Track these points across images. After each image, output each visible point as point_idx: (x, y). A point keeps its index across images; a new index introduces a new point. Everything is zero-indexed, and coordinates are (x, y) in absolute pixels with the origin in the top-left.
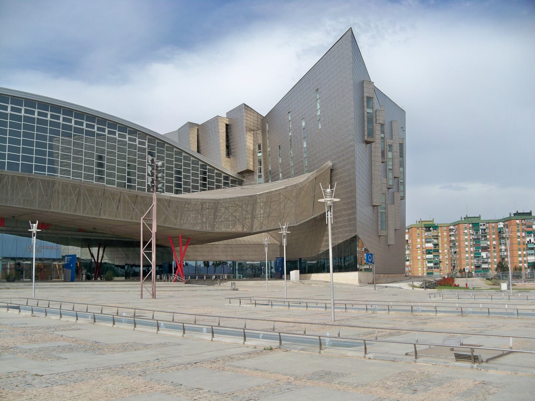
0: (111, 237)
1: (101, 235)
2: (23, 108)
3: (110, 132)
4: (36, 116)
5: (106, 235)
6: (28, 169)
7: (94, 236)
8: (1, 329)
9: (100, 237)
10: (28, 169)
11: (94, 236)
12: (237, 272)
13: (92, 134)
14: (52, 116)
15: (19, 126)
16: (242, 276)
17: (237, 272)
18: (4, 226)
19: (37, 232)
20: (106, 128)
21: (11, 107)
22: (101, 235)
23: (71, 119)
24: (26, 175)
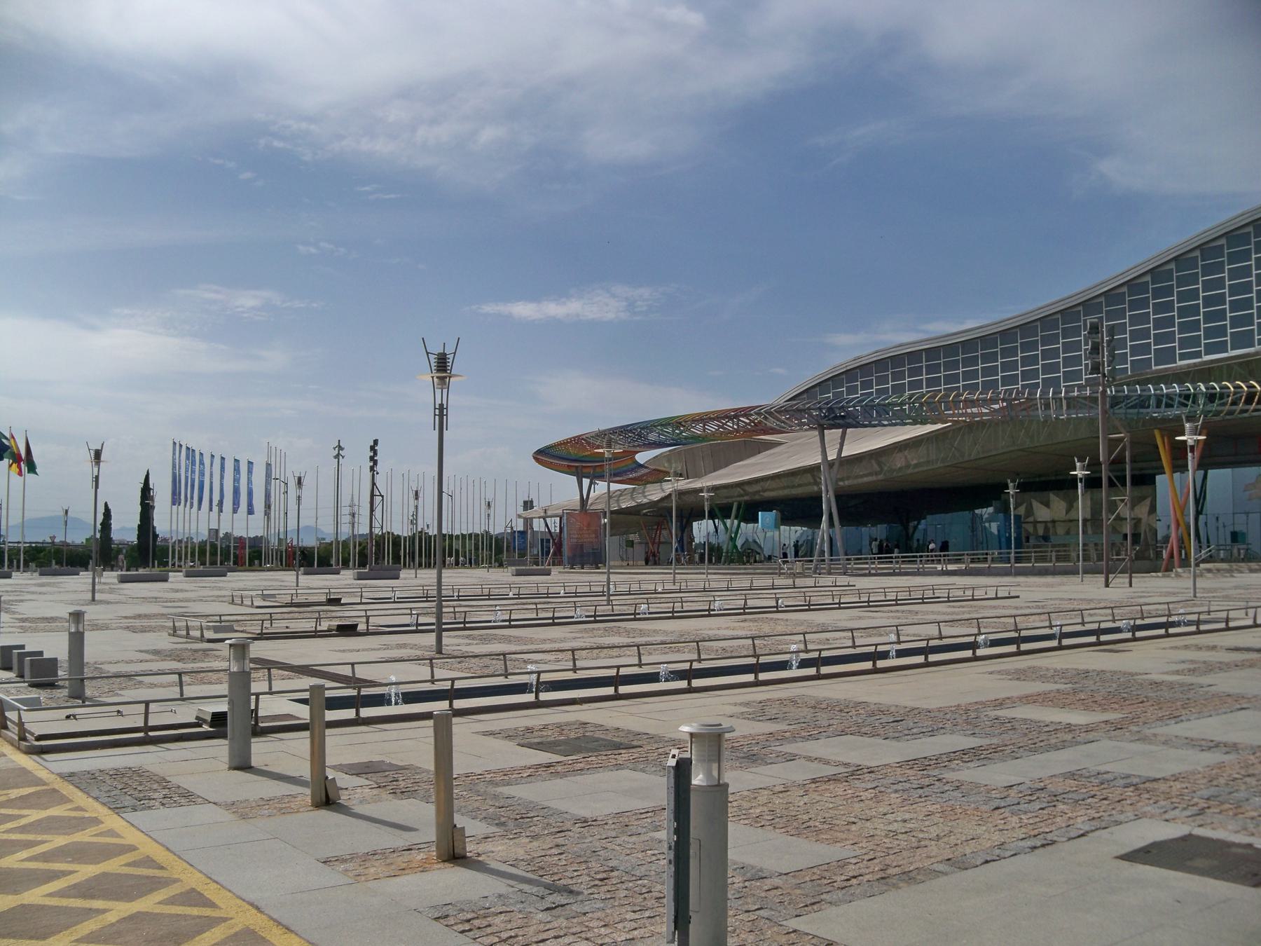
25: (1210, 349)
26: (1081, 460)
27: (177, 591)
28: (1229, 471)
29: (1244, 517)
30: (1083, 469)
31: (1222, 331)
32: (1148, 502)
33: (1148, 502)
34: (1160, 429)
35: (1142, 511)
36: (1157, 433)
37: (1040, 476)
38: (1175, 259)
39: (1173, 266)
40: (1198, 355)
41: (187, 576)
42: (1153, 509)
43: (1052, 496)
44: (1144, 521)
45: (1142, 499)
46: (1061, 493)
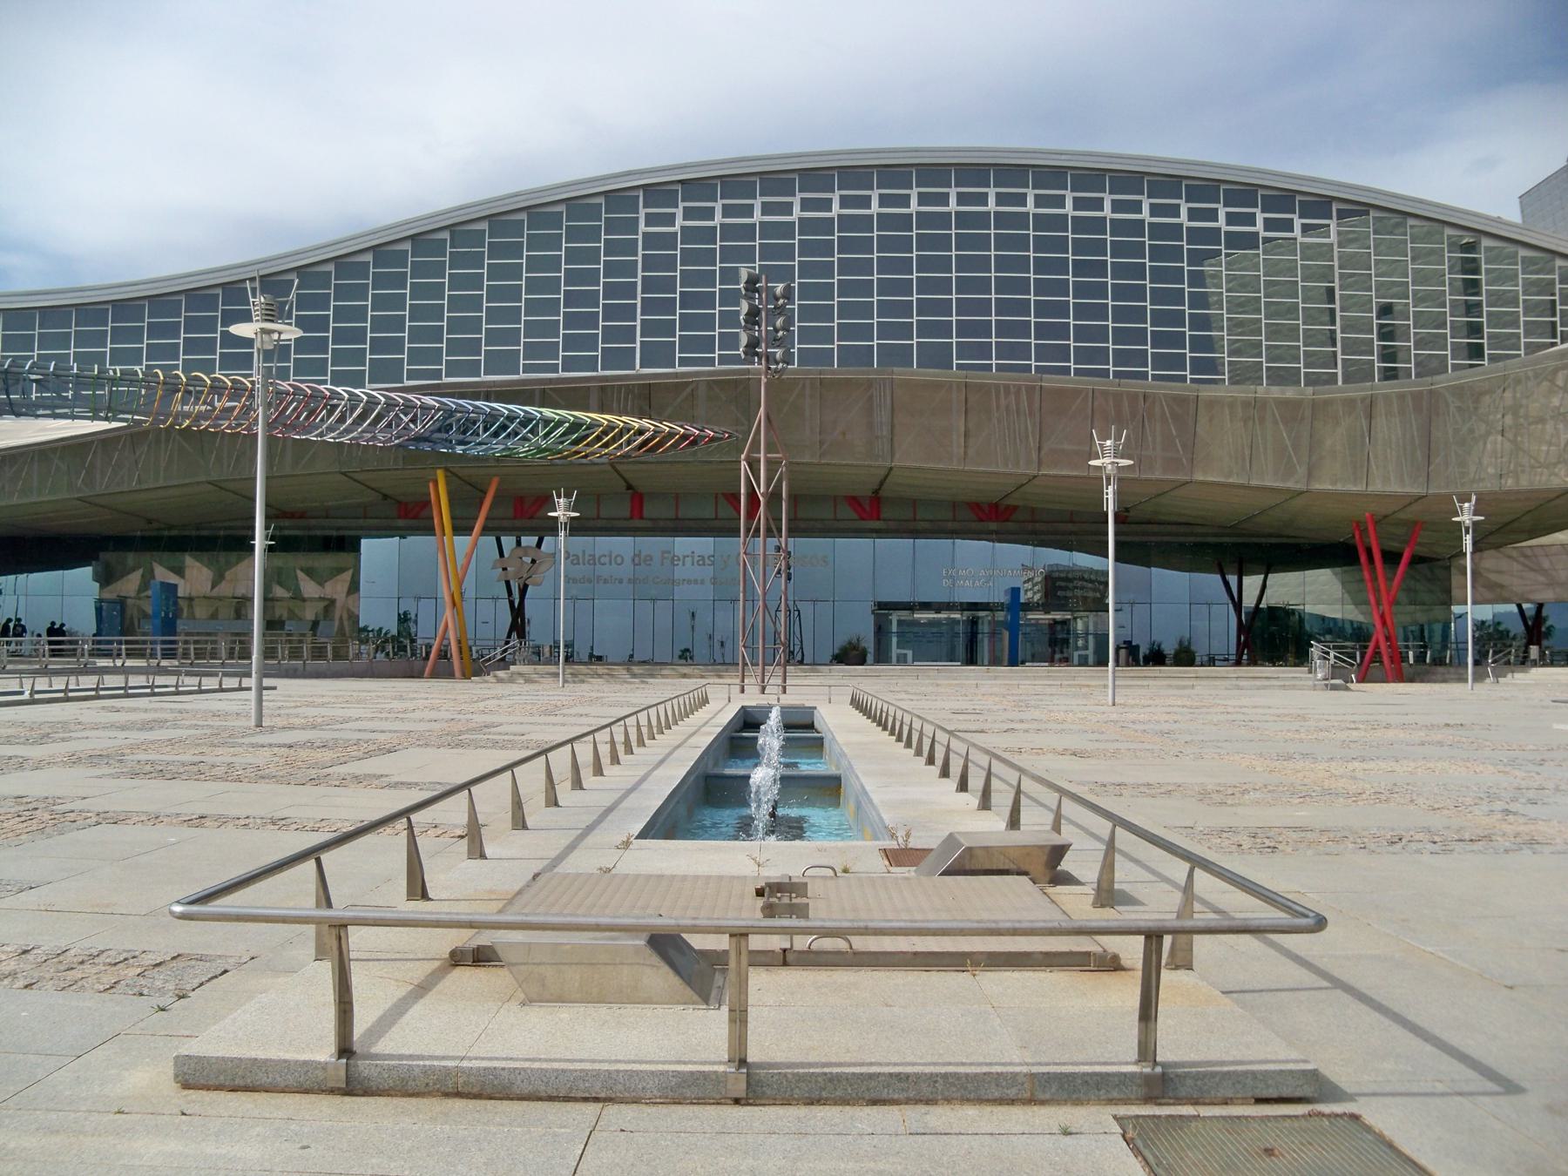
0: (1215, 535)
1: (1182, 529)
2: (914, 194)
3: (1231, 220)
4: (953, 206)
5: (1200, 530)
6: (937, 357)
7: (1155, 534)
8: (2, 811)
9: (1177, 535)
10: (937, 357)
11: (1155, 534)
12: (894, 640)
13: (1251, 241)
14: (1117, 206)
15: (1138, 250)
16: (910, 653)
17: (894, 640)
18: (641, 518)
19: (1475, 523)
20: (1258, 211)
21: (1036, 196)
22: (1182, 529)
23: (1037, 206)
24: (933, 374)
25: (569, 364)
26: (568, 496)
27: (146, 726)
28: (628, 540)
29: (649, 604)
30: (568, 509)
31: (590, 342)
32: (347, 576)
33: (347, 576)
34: (447, 469)
35: (337, 588)
36: (440, 475)
37: (171, 528)
38: (412, 238)
39: (407, 246)
40: (554, 368)
41: (523, 1004)
42: (354, 587)
43: (189, 560)
44: (338, 604)
45: (341, 570)
46: (205, 556)
